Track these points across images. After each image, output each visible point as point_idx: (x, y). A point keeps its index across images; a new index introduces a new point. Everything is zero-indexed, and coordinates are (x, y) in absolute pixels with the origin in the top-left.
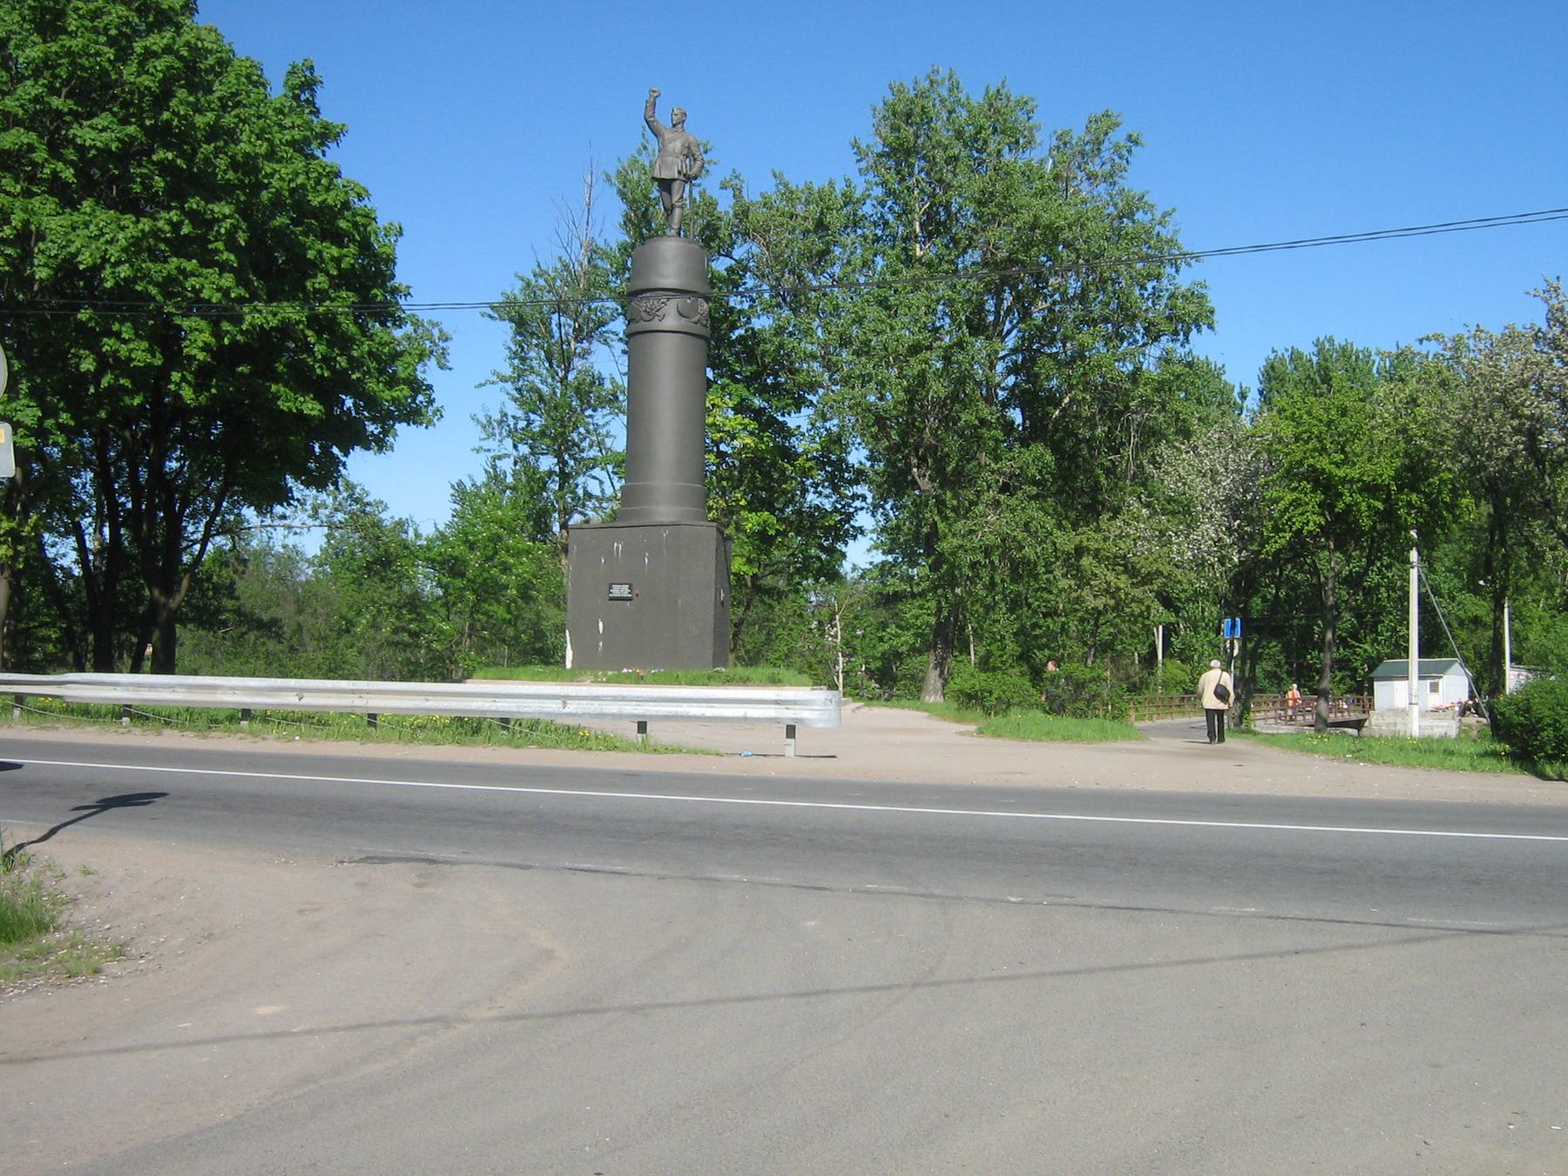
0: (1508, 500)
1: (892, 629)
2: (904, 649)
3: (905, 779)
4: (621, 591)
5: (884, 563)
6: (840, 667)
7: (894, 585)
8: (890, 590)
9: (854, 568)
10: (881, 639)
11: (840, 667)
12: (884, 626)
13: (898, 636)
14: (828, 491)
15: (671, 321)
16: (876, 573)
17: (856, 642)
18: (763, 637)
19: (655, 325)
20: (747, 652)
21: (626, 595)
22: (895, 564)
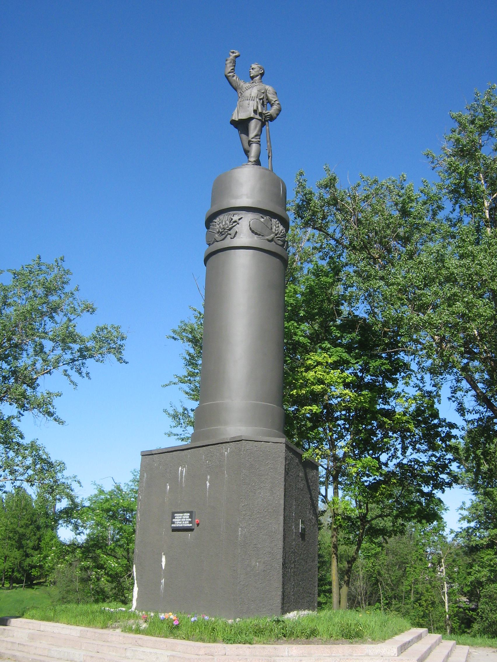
0: (152, 614)
1: (476, 568)
2: (484, 579)
3: (249, 128)
4: (182, 520)
5: (469, 528)
6: (446, 590)
7: (476, 540)
8: (474, 543)
9: (452, 532)
10: (469, 574)
11: (446, 590)
12: (471, 566)
13: (479, 571)
14: (424, 447)
15: (244, 237)
16: (464, 534)
17: (455, 575)
18: (401, 572)
19: (228, 242)
20: (392, 581)
21: (187, 525)
22: (475, 529)
